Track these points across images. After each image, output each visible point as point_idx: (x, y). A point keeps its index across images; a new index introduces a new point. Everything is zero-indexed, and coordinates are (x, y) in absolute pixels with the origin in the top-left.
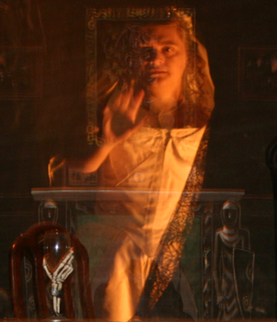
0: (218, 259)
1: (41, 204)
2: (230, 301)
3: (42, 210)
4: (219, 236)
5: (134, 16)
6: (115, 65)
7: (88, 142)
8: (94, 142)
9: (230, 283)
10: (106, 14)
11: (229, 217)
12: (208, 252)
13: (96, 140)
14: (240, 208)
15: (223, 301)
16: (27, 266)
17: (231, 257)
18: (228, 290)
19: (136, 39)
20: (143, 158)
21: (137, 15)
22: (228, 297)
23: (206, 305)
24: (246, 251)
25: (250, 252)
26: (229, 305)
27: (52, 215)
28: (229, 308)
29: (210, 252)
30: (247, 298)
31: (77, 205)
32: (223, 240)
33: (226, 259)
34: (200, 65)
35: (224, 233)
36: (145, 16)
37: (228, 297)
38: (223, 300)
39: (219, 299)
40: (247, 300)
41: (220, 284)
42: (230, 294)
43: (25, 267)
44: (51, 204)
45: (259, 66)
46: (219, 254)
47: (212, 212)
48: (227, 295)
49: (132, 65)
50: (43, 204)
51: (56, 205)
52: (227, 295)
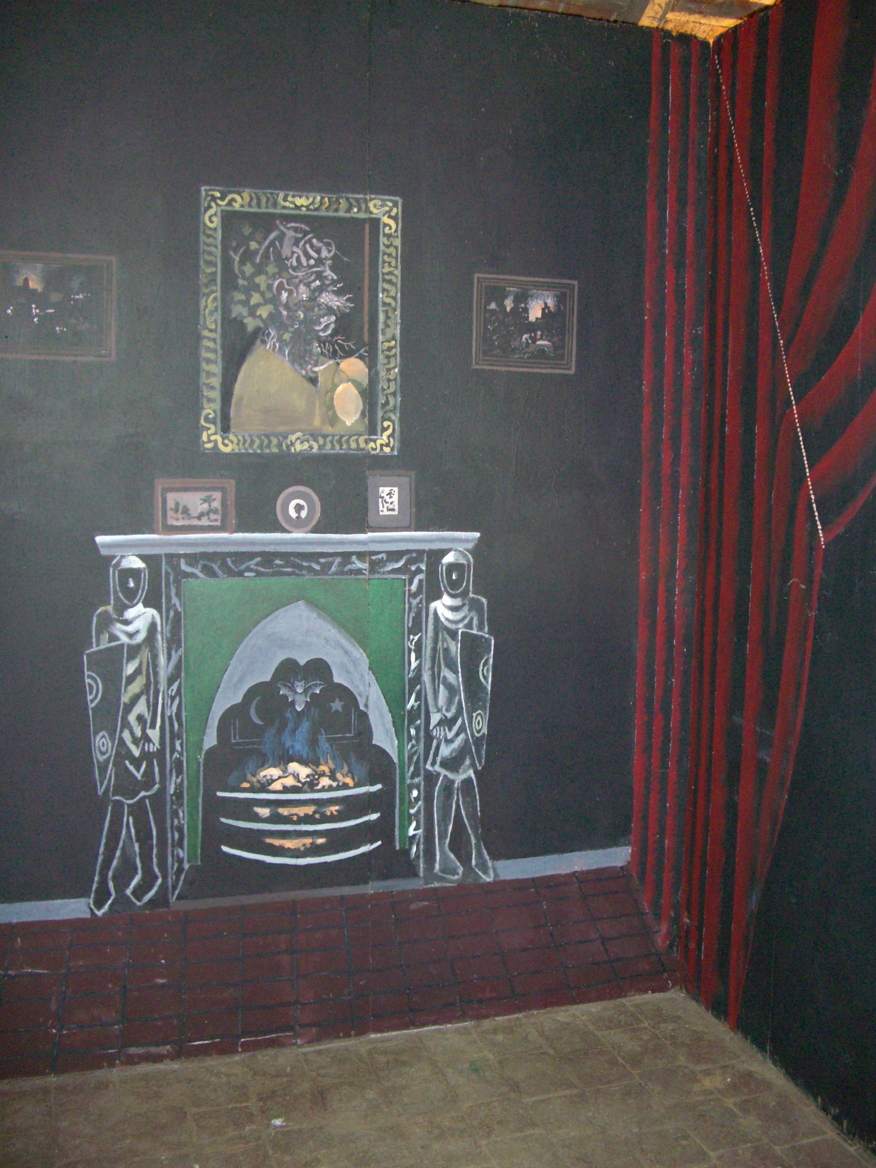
0: (434, 650)
1: (114, 562)
2: (454, 720)
3: (117, 572)
4: (436, 613)
5: (292, 206)
6: (256, 298)
7: (204, 443)
8: (216, 442)
9: (452, 690)
10: (240, 201)
11: (454, 577)
12: (416, 638)
13: (220, 440)
14: (472, 560)
15: (440, 723)
16: (90, 677)
17: (455, 648)
18: (450, 702)
19: (295, 249)
20: (389, 322)
21: (298, 204)
22: (449, 715)
23: (413, 732)
24: (480, 633)
25: (487, 636)
26: (450, 730)
27: (137, 584)
28: (450, 735)
29: (420, 639)
30: (480, 714)
31: (182, 561)
32: (443, 619)
33: (447, 650)
34: (295, 818)
35: (443, 607)
36: (311, 207)
37: (449, 715)
38: (441, 720)
39: (435, 718)
40: (479, 718)
41: (436, 693)
42: (453, 710)
43: (87, 681)
44: (136, 563)
45: (508, 309)
46: (436, 640)
47: (424, 568)
48: (447, 710)
49: (288, 297)
50: (119, 563)
51: (642, 27)
52: (447, 710)
